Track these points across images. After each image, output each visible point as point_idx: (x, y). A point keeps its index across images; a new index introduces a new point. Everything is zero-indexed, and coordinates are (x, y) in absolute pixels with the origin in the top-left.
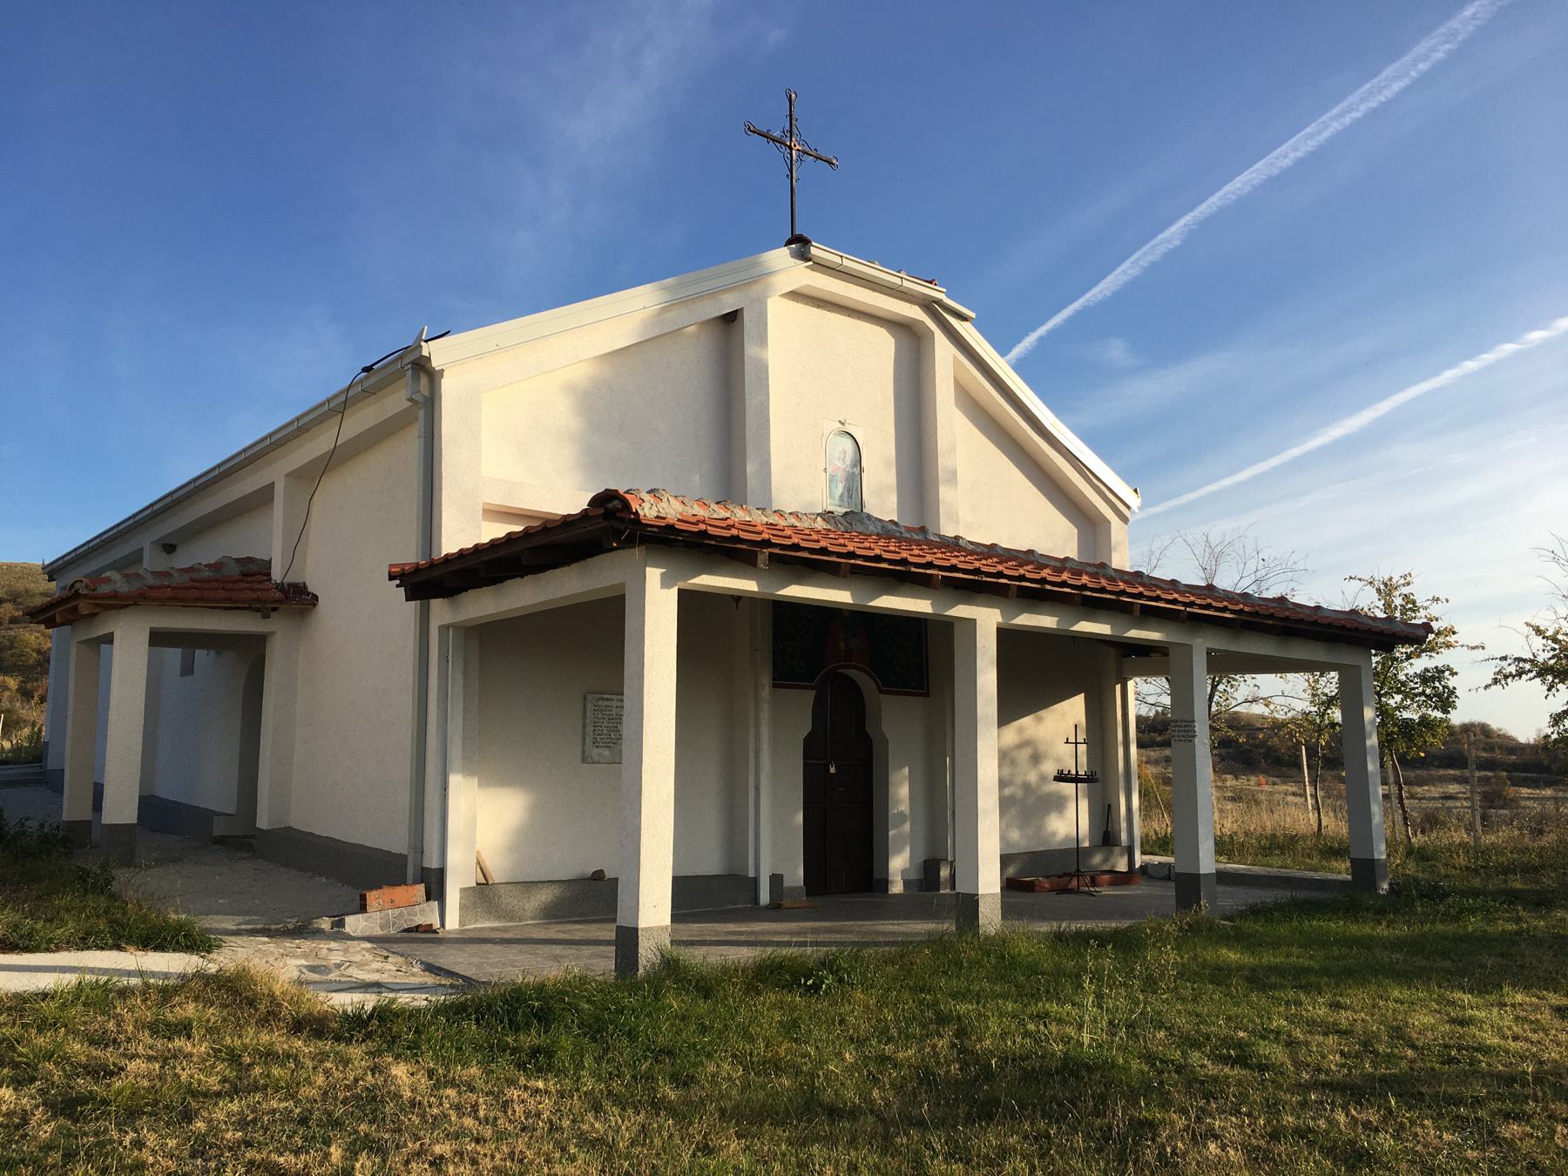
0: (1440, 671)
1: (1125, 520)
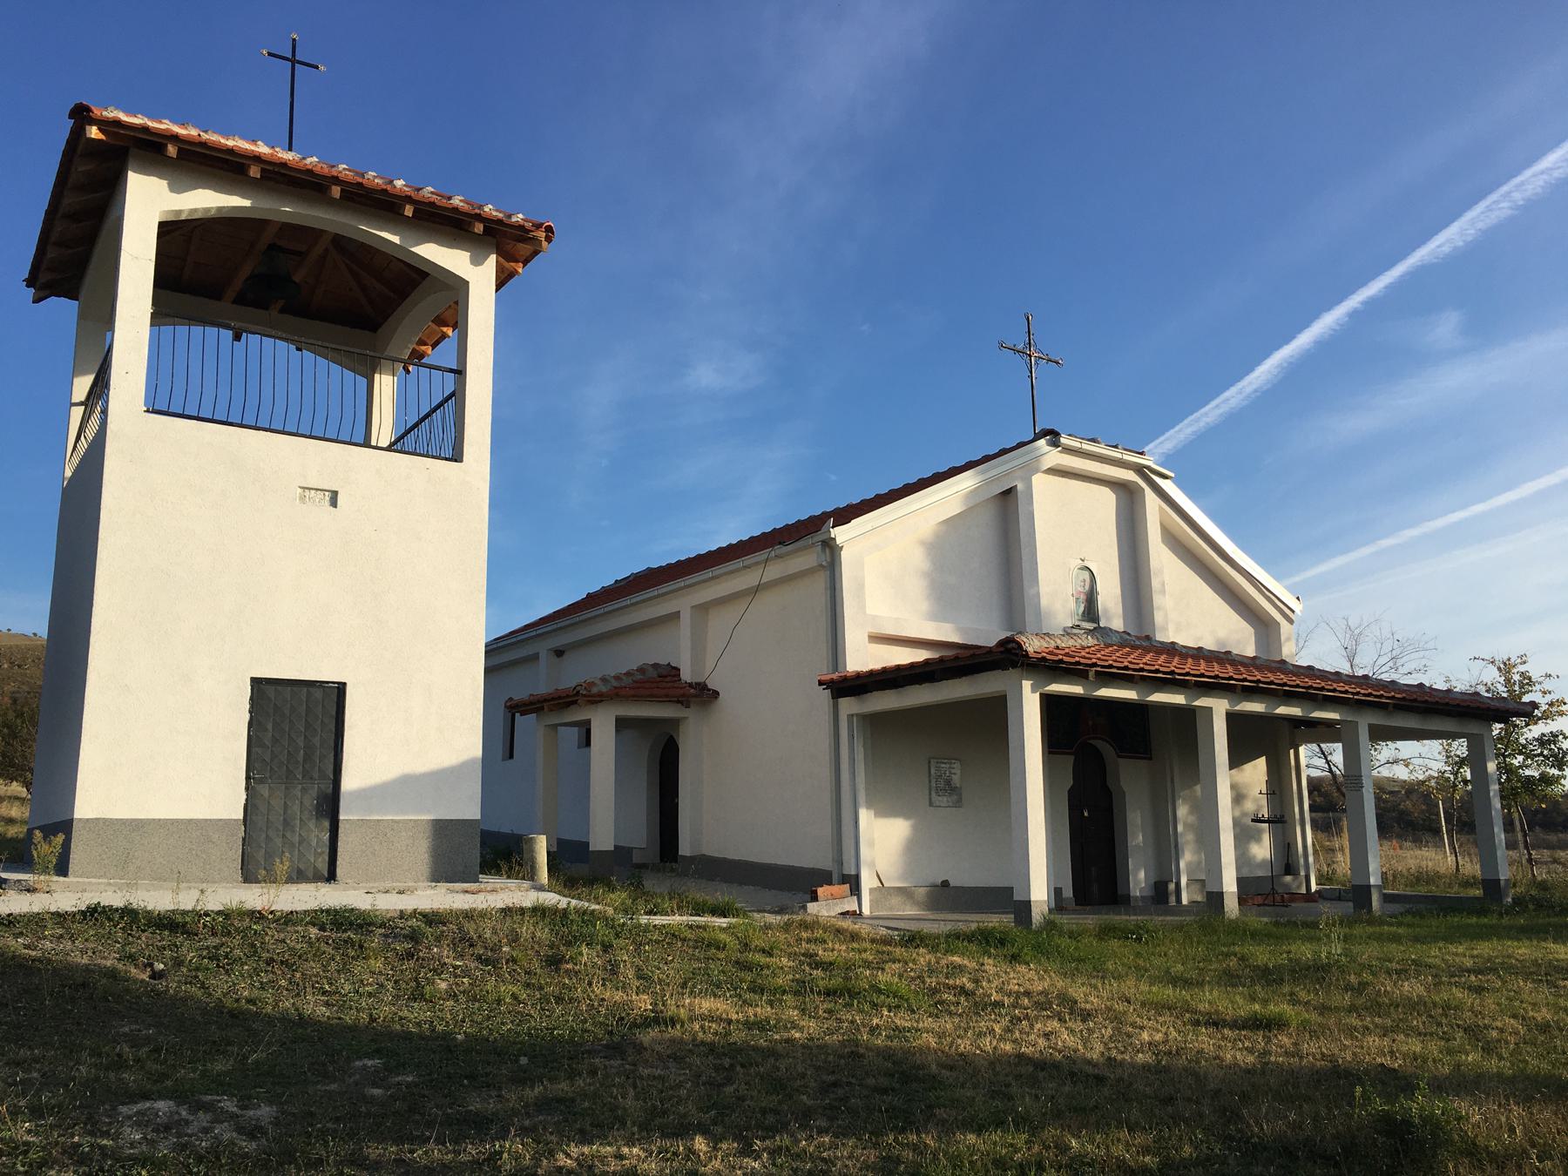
0: (1554, 735)
1: (1291, 621)
